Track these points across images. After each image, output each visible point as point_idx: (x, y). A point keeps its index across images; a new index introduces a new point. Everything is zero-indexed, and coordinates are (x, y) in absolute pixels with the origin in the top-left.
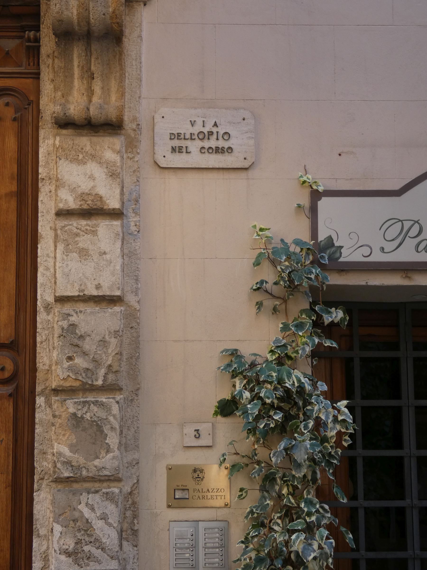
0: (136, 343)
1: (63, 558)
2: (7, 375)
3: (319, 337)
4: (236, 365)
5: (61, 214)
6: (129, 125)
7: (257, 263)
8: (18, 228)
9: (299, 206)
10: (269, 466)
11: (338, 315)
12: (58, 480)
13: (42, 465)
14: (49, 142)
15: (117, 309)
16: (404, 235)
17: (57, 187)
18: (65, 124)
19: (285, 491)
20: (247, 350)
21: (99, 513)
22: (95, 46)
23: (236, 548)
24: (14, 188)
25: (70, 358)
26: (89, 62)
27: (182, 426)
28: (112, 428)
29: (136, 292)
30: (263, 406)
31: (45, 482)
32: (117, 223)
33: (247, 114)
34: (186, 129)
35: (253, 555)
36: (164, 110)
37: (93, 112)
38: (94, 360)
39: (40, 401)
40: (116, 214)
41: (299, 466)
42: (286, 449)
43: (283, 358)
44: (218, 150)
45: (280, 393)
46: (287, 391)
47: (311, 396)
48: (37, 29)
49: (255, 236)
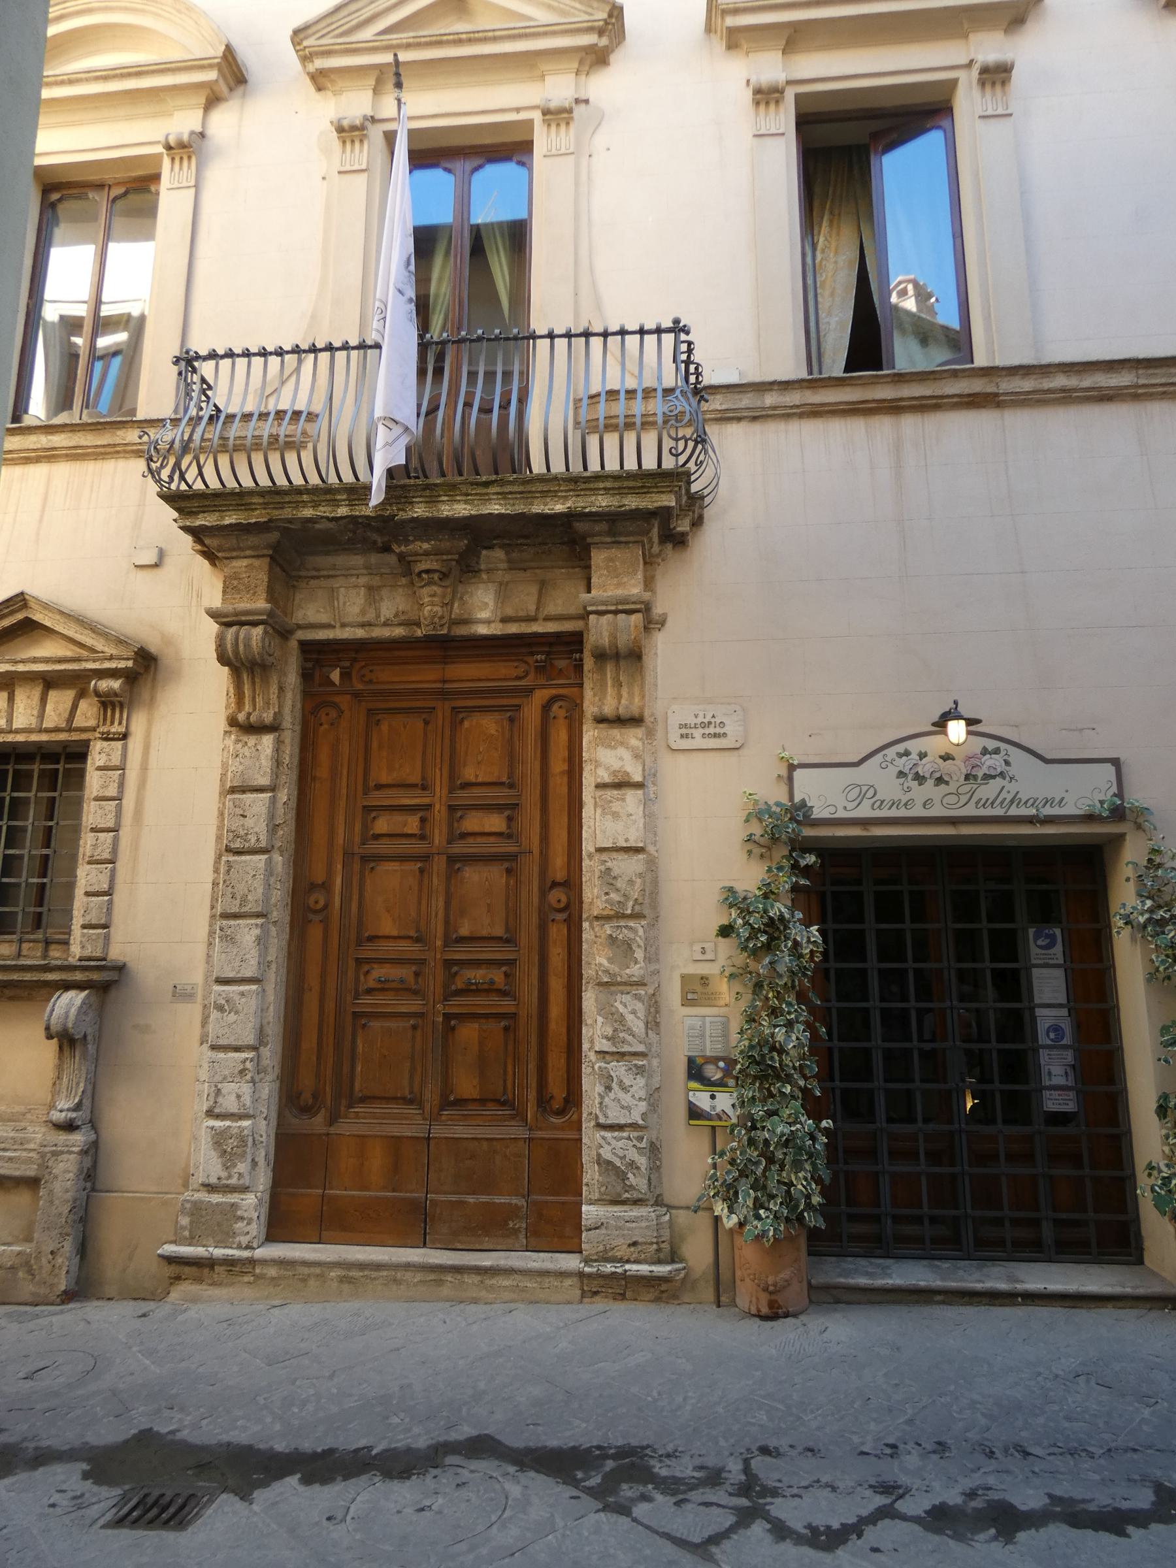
0: (655, 882)
1: (604, 1041)
2: (562, 905)
3: (797, 876)
4: (732, 898)
5: (599, 786)
6: (648, 719)
7: (747, 821)
8: (569, 845)
9: (779, 776)
10: (759, 974)
11: (811, 859)
12: (600, 984)
13: (588, 972)
14: (589, 733)
15: (641, 856)
16: (862, 796)
17: (596, 767)
18: (601, 720)
19: (770, 995)
20: (740, 887)
21: (630, 1008)
22: (622, 663)
23: (734, 1037)
24: (566, 768)
25: (607, 894)
26: (618, 675)
27: (691, 945)
28: (639, 946)
29: (655, 843)
30: (753, 930)
31: (590, 985)
32: (640, 792)
33: (737, 708)
34: (691, 720)
35: (746, 1043)
36: (675, 707)
37: (621, 711)
38: (624, 895)
39: (585, 925)
40: (639, 786)
41: (780, 976)
42: (770, 963)
43: (768, 894)
44: (715, 735)
45: (765, 920)
46: (771, 918)
47: (789, 922)
48: (582, 652)
49: (745, 800)
